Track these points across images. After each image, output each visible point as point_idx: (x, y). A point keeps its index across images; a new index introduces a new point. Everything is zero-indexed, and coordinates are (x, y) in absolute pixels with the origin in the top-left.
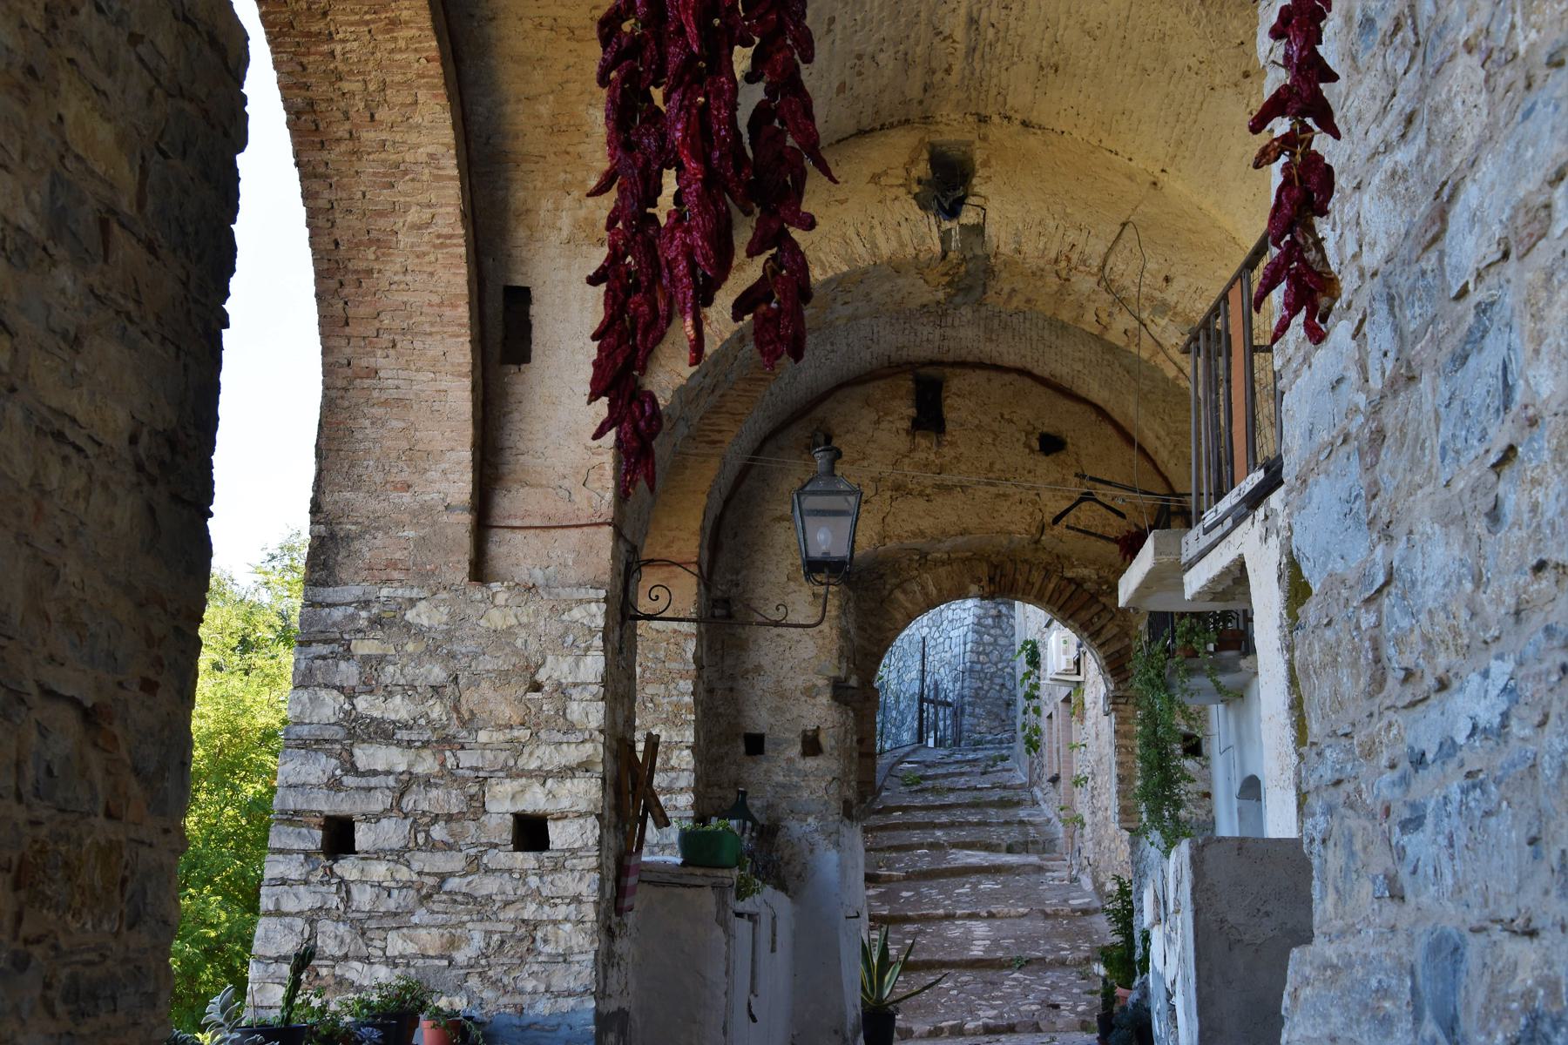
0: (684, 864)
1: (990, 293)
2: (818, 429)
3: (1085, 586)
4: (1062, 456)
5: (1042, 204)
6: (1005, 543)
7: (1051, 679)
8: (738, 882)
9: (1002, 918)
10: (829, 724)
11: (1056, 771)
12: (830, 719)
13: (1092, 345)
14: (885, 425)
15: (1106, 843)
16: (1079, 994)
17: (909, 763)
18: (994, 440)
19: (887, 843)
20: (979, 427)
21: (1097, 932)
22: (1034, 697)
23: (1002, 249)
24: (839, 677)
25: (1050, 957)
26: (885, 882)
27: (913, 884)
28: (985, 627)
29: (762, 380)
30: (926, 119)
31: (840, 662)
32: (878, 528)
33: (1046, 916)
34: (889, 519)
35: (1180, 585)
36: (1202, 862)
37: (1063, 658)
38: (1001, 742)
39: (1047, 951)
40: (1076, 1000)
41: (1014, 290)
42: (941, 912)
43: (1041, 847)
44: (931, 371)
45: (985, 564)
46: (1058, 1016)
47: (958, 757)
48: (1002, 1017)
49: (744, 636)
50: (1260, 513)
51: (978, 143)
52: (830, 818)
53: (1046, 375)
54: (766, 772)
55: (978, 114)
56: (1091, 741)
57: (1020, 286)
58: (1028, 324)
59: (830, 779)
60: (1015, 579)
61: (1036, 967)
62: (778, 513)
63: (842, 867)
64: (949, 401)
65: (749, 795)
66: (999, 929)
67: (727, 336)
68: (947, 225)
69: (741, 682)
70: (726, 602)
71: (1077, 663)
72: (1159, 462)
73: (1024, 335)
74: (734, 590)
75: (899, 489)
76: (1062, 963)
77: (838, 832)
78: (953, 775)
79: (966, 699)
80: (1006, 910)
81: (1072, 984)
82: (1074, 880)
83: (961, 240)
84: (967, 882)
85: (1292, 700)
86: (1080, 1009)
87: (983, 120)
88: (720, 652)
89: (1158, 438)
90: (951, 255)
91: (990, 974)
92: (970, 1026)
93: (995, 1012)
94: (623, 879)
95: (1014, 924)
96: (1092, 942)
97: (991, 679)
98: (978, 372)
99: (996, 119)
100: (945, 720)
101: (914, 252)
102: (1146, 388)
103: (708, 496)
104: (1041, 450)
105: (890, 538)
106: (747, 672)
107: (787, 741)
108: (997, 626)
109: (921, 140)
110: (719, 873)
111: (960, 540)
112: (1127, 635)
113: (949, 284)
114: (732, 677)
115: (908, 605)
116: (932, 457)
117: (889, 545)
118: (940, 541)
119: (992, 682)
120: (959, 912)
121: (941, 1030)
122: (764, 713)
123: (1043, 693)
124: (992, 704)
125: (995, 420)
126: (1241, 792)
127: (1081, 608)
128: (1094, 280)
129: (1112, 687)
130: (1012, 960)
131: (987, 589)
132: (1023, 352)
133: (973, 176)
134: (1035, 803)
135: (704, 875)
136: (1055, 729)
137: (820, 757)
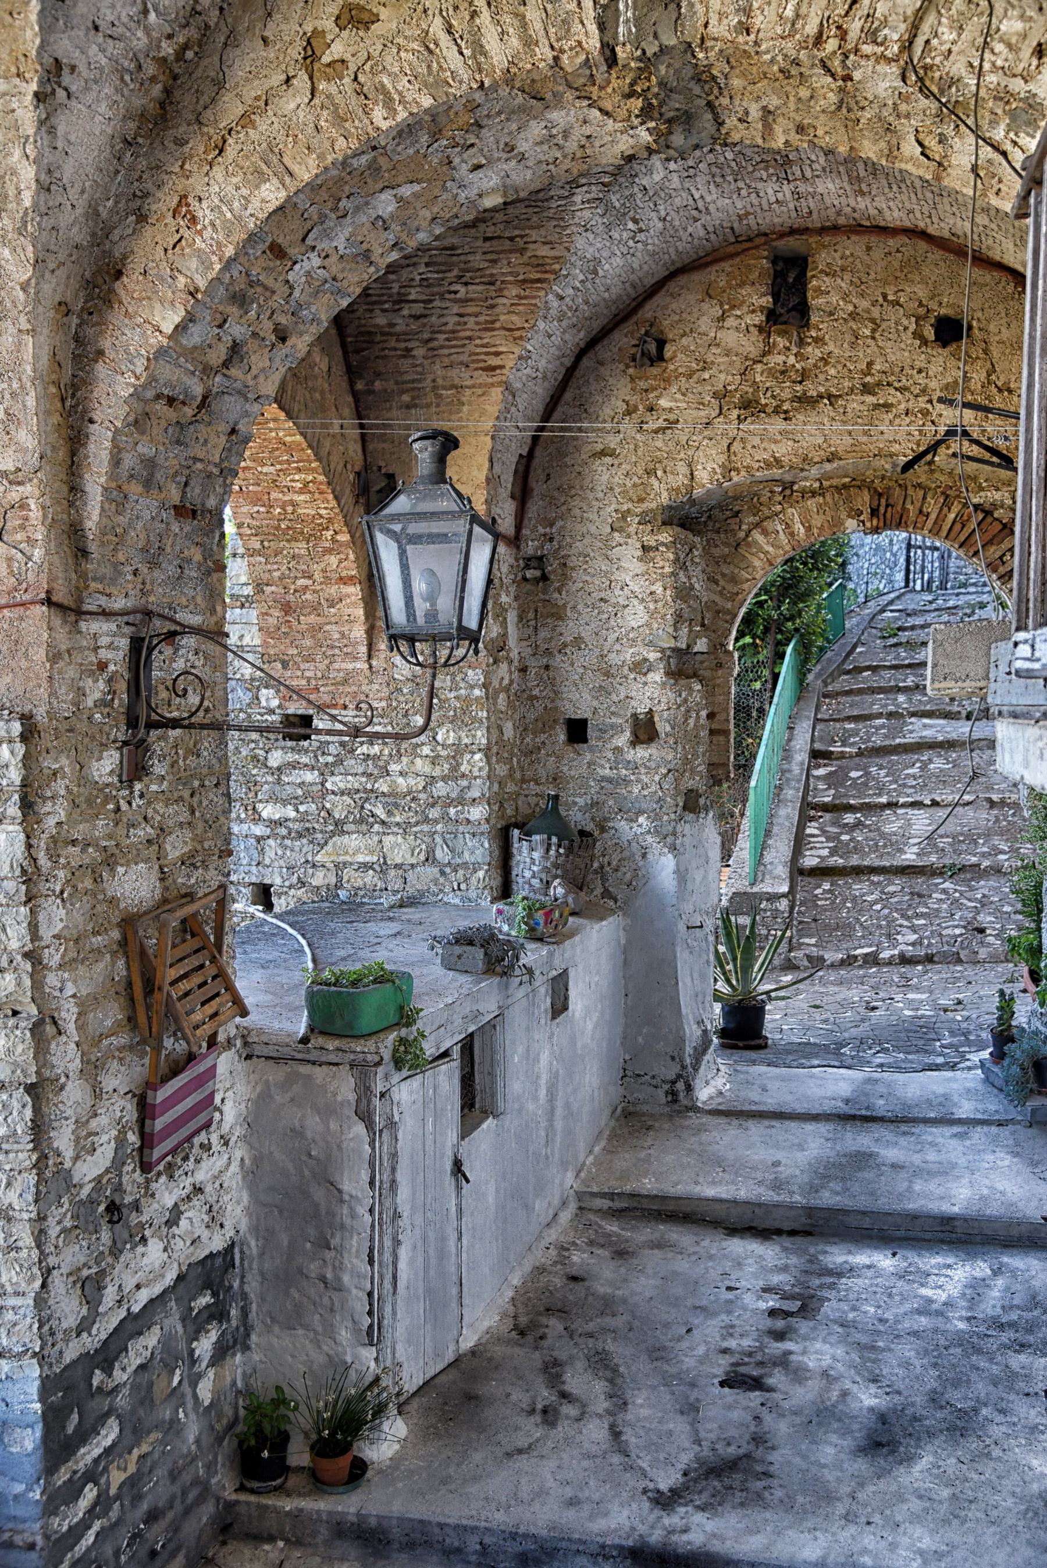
1: (731, 122)
2: (647, 333)
10: (663, 706)
12: (664, 700)
14: (731, 322)
17: (892, 611)
18: (874, 331)
19: (848, 712)
25: (986, 863)
26: (837, 759)
29: (539, 281)
32: (722, 459)
34: (736, 447)
42: (884, 800)
45: (866, 492)
49: (561, 603)
52: (666, 818)
59: (664, 771)
60: (904, 508)
62: (599, 447)
65: (562, 800)
69: (559, 658)
70: (540, 561)
73: (903, 181)
75: (750, 406)
88: (533, 623)
92: (885, 955)
94: (148, 1122)
98: (854, 238)
101: (550, 54)
103: (493, 438)
105: (738, 470)
107: (612, 726)
111: (828, 466)
113: (646, 113)
115: (770, 549)
116: (792, 360)
117: (736, 479)
118: (802, 470)
120: (902, 800)
121: (856, 957)
122: (586, 696)
128: (894, 70)
131: (868, 525)
132: (908, 205)
135: (338, 1049)
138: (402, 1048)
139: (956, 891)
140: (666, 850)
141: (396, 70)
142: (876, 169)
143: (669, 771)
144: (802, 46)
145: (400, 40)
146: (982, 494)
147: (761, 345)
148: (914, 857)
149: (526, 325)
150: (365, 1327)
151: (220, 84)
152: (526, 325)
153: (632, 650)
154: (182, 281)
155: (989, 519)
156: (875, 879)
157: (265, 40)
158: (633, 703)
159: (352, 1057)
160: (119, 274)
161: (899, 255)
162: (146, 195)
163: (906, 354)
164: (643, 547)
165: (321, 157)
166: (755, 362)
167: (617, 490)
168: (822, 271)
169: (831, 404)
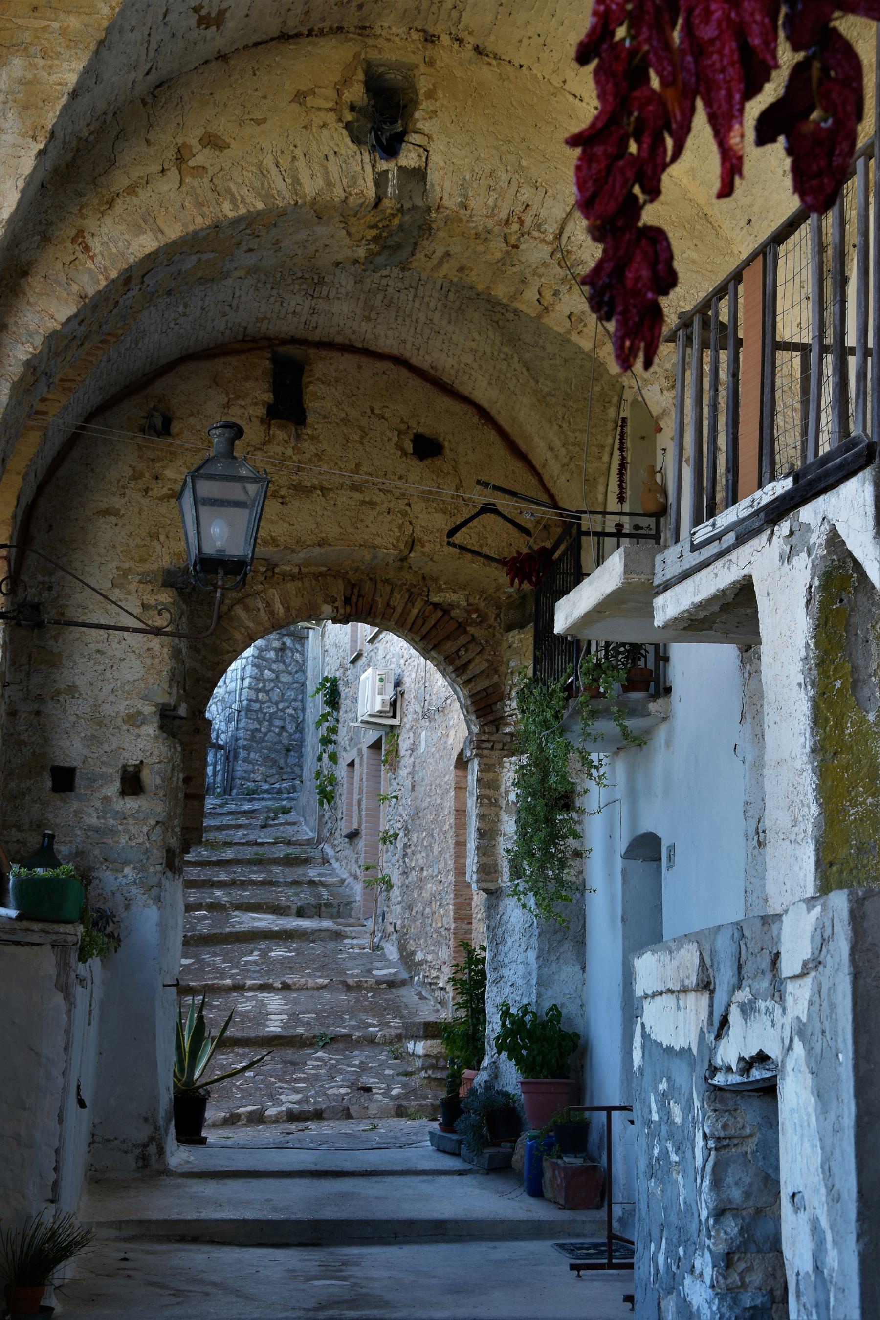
0: (19, 918)
1: (419, 255)
2: (154, 408)
3: (453, 613)
4: (438, 462)
5: (494, 151)
6: (368, 558)
7: (363, 722)
8: (83, 940)
9: (298, 989)
10: (155, 759)
11: (355, 826)
12: (156, 753)
13: (491, 334)
15: (419, 907)
16: (392, 1076)
18: (362, 437)
20: (345, 421)
21: (406, 1007)
22: (331, 742)
23: (446, 202)
24: (169, 704)
25: (357, 1034)
27: (192, 950)
28: (266, 660)
30: (363, 30)
31: (170, 687)
33: (349, 988)
35: (649, 614)
36: (863, 917)
37: (379, 699)
38: (279, 792)
39: (353, 1027)
40: (390, 1082)
41: (448, 254)
42: (228, 982)
43: (335, 910)
44: (293, 351)
45: (340, 582)
46: (370, 1100)
47: (232, 807)
48: (307, 1102)
49: (56, 650)
50: (784, 527)
51: (423, 68)
52: (152, 869)
53: (425, 366)
54: (76, 813)
55: (424, 31)
56: (404, 792)
57: (455, 249)
58: (417, 305)
59: (153, 822)
60: (373, 600)
61: (341, 1046)
62: (104, 506)
63: (163, 927)
64: (311, 388)
66: (296, 1002)
67: (114, 274)
68: (383, 165)
69: (51, 704)
71: (394, 704)
72: (546, 478)
73: (410, 316)
74: (46, 595)
76: (371, 1041)
77: (159, 885)
78: (229, 827)
79: (241, 742)
80: (303, 980)
81: (383, 1064)
82: (377, 948)
83: (399, 187)
84: (255, 949)
85: (815, 743)
86: (394, 1092)
87: (430, 39)
88: (26, 667)
89: (551, 448)
90: (386, 203)
91: (290, 1053)
92: (271, 1112)
93: (298, 1096)
95: (311, 997)
96: (402, 1017)
97: (270, 721)
98: (348, 356)
99: (445, 39)
100: (215, 765)
101: (343, 195)
102: (546, 390)
103: (24, 479)
104: (415, 453)
106: (58, 693)
107: (102, 776)
108: (280, 660)
109: (356, 56)
110: (62, 928)
111: (317, 551)
112: (496, 671)
113: (375, 239)
114: (40, 698)
115: (251, 625)
116: (289, 452)
118: (293, 551)
119: (271, 724)
120: (249, 982)
121: (239, 1116)
122: (77, 743)
123: (342, 736)
124: (270, 749)
125: (363, 414)
126: (627, 851)
127: (447, 638)
129: (476, 730)
130: (314, 1037)
131: (342, 611)
133: (415, 110)
134: (325, 861)
136: (357, 778)
137: (142, 796)
138: (88, 939)
139: (331, 1059)
140: (151, 902)
141: (240, 181)
142: (391, 302)
143: (158, 823)
144: (499, 224)
145: (244, 163)
146: (442, 594)
147: (263, 434)
148: (279, 1029)
149: (78, 378)
150: (50, 1183)
151: (112, 162)
152: (78, 378)
153: (127, 703)
154: (75, 288)
155: (446, 618)
156: (240, 1051)
157: (148, 141)
158: (125, 754)
159: (54, 937)
160: (25, 274)
161: (385, 377)
162: (50, 224)
163: (389, 461)
164: (143, 605)
165: (185, 225)
166: (256, 449)
167: (120, 548)
168: (318, 379)
169: (323, 495)
